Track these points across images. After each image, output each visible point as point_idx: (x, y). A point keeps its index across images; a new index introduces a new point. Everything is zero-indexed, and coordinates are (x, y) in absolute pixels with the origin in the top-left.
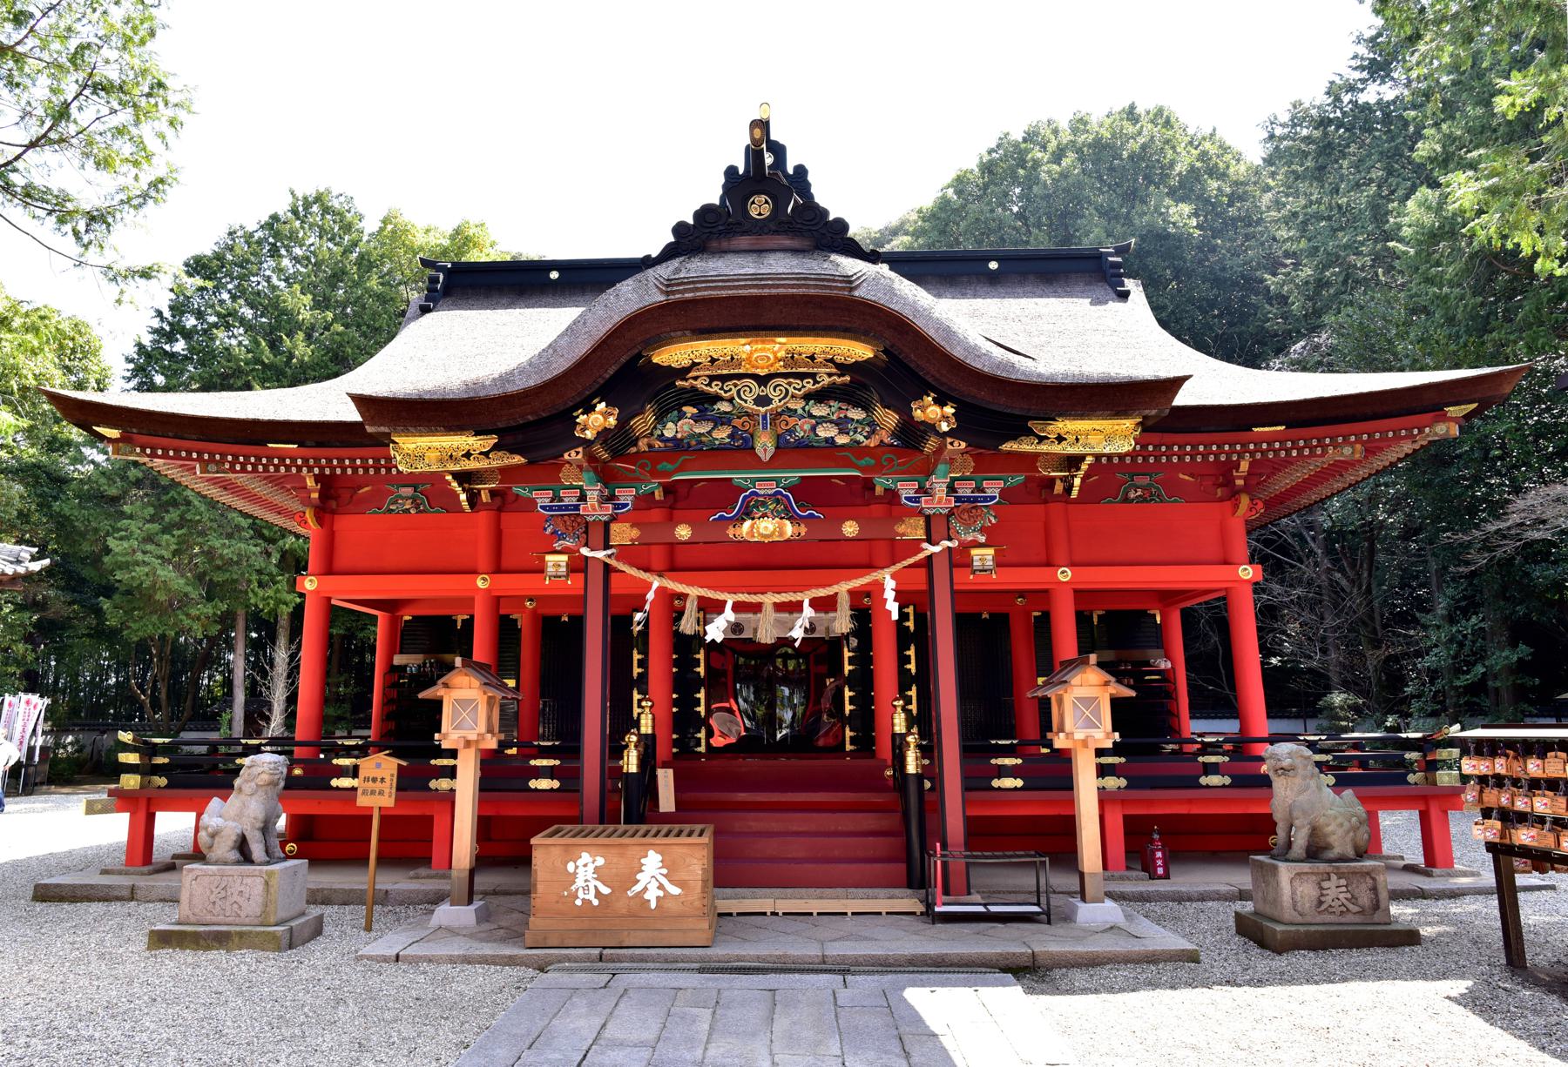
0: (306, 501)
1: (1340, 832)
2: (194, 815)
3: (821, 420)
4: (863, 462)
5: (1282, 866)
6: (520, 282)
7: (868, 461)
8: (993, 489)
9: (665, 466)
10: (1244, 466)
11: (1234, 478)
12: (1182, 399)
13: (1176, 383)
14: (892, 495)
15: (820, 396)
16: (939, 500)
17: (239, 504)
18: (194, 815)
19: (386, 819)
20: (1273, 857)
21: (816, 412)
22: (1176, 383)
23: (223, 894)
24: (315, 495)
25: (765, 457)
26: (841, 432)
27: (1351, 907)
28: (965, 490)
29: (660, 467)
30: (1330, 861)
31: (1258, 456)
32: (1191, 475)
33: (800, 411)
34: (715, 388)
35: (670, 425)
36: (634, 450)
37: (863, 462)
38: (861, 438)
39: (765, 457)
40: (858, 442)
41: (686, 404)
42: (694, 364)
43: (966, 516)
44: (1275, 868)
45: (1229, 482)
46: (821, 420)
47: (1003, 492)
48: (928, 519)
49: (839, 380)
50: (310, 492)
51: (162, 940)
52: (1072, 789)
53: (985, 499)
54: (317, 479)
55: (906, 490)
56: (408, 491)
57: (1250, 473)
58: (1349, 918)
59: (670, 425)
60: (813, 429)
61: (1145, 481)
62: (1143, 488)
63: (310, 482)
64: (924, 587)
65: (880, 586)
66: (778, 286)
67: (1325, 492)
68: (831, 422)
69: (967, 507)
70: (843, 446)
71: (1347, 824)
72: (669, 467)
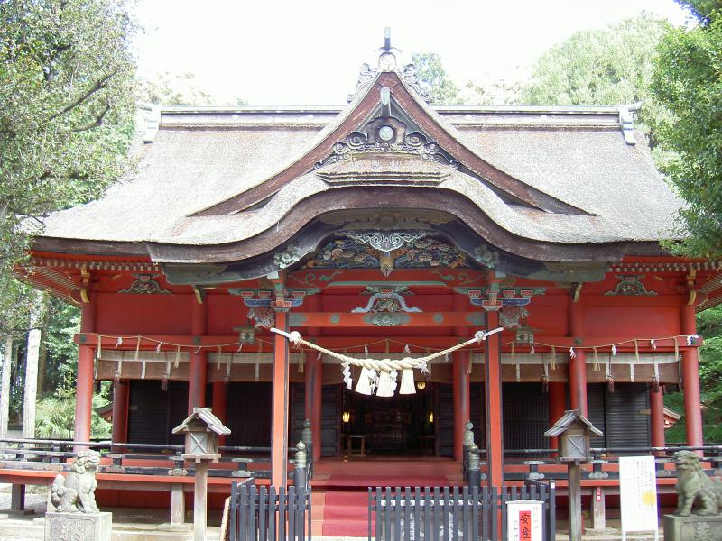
2: (401, 392)
4: (447, 278)
6: (258, 121)
7: (449, 277)
8: (527, 297)
9: (324, 278)
10: (693, 273)
16: (492, 305)
17: (55, 442)
18: (401, 392)
24: (86, 281)
25: (387, 274)
26: (434, 259)
28: (510, 296)
29: (320, 279)
36: (305, 267)
37: (447, 278)
38: (445, 262)
39: (387, 274)
40: (445, 265)
43: (509, 312)
46: (422, 251)
47: (532, 299)
48: (486, 314)
52: (620, 519)
54: (88, 270)
55: (474, 297)
56: (146, 279)
60: (417, 256)
61: (629, 280)
63: (84, 273)
65: (510, 345)
68: (428, 252)
69: (509, 308)
70: (434, 267)
72: (326, 278)
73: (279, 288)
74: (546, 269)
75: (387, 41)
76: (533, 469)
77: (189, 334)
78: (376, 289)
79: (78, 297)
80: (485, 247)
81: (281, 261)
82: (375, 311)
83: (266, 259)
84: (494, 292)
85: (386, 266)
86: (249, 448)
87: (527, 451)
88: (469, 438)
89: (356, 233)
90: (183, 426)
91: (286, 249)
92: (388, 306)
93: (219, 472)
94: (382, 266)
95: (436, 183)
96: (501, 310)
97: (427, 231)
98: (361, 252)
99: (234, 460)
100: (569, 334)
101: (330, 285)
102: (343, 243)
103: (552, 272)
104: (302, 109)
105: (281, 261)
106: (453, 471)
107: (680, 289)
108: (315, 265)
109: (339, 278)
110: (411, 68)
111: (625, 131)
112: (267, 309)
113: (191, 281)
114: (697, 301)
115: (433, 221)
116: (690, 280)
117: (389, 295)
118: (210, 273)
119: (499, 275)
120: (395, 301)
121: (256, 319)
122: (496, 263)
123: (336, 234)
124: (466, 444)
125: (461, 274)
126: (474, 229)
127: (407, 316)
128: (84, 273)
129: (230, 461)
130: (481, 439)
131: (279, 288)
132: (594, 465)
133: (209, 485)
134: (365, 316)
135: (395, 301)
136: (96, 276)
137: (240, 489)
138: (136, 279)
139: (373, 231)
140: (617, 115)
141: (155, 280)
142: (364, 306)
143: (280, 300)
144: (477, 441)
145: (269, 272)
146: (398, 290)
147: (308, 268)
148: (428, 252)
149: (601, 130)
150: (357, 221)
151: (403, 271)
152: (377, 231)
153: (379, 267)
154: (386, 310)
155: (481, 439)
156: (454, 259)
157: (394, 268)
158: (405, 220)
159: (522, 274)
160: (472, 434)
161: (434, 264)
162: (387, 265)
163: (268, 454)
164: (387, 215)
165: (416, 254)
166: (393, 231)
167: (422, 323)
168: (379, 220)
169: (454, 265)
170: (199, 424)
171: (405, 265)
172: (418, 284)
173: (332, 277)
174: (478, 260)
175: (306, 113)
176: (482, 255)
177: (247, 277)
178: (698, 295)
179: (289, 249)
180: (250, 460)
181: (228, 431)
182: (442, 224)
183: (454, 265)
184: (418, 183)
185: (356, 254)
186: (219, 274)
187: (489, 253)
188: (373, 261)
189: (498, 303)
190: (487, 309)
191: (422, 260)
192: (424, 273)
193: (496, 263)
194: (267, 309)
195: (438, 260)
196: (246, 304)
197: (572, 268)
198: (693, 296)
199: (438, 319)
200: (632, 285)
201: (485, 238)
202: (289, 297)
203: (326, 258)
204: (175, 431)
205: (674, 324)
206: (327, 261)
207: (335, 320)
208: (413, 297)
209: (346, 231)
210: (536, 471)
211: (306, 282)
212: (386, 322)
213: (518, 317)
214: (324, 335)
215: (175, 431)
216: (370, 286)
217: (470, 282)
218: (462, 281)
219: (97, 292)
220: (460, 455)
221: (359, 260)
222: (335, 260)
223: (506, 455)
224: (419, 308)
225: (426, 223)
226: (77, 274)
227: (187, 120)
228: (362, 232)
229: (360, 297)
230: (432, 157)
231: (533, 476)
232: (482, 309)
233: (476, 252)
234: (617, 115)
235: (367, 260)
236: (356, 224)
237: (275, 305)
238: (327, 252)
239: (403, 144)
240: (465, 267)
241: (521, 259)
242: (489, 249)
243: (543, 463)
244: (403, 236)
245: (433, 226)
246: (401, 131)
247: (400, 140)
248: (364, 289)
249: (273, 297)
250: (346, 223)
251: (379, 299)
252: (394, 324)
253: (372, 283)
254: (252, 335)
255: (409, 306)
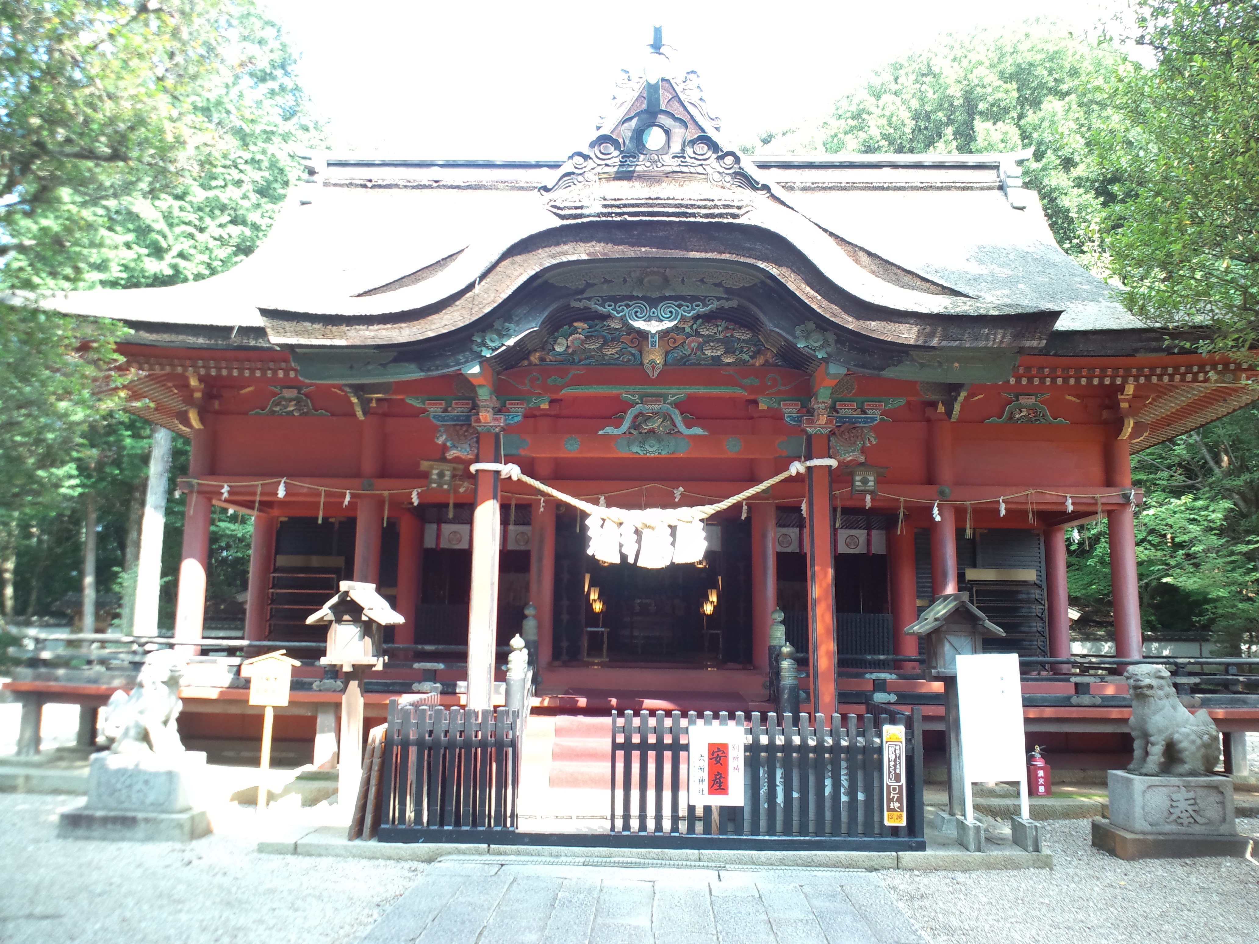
0: (189, 400)
1: (1193, 748)
3: (708, 339)
5: (1136, 778)
8: (875, 412)
10: (1130, 389)
11: (1118, 403)
12: (1062, 325)
13: (1056, 315)
14: (776, 416)
15: (707, 318)
16: (821, 424)
19: (280, 719)
20: (1129, 772)
21: (704, 332)
22: (1056, 315)
23: (128, 782)
24: (198, 395)
26: (727, 352)
27: (1198, 819)
28: (848, 411)
29: (549, 381)
30: (1181, 775)
31: (1142, 380)
32: (1076, 396)
33: (688, 330)
34: (607, 309)
35: (561, 340)
36: (526, 363)
37: (747, 382)
38: (746, 357)
40: (745, 362)
41: (576, 321)
42: (589, 285)
44: (1129, 781)
45: (1114, 406)
46: (708, 339)
48: (809, 437)
49: (726, 304)
50: (192, 391)
51: (75, 823)
53: (866, 420)
54: (201, 379)
55: (790, 411)
57: (1134, 396)
58: (1197, 829)
59: (561, 340)
60: (700, 347)
61: (1028, 401)
62: (1029, 409)
63: (194, 382)
64: (524, 826)
66: (693, 215)
67: (1212, 416)
68: (718, 340)
69: (845, 429)
70: (729, 364)
71: (1199, 742)
72: (560, 382)
73: (484, 394)
74: (913, 360)
75: (658, 32)
76: (880, 686)
77: (357, 475)
78: (636, 398)
79: (184, 420)
80: (811, 325)
81: (484, 344)
82: (635, 432)
83: (460, 340)
84: (823, 397)
85: (652, 362)
86: (440, 647)
87: (869, 657)
88: (778, 634)
89: (605, 300)
90: (325, 612)
91: (492, 326)
92: (655, 424)
93: (393, 684)
94: (646, 361)
95: (735, 216)
96: (832, 433)
97: (719, 299)
98: (613, 340)
99: (416, 665)
100: (930, 479)
101: (564, 391)
102: (586, 326)
103: (922, 366)
104: (533, 159)
105: (484, 344)
106: (749, 682)
107: (1105, 414)
108: (542, 359)
109: (578, 381)
110: (692, 76)
111: (1008, 190)
112: (465, 427)
113: (339, 380)
114: (1136, 433)
115: (729, 284)
116: (1125, 401)
117: (656, 407)
118: (368, 363)
119: (836, 370)
120: (667, 417)
121: (449, 444)
122: (829, 349)
123: (575, 304)
124: (775, 643)
125: (769, 376)
126: (797, 293)
127: (685, 440)
128: (194, 382)
129: (411, 667)
130: (799, 634)
131: (484, 394)
132: (1077, 685)
133: (366, 705)
134: (619, 440)
135: (667, 417)
136: (214, 389)
137: (405, 713)
138: (275, 394)
139: (632, 298)
140: (997, 167)
141: (305, 395)
142: (617, 426)
143: (486, 416)
144: (789, 638)
145: (466, 362)
146: (671, 399)
147: (530, 364)
148: (718, 340)
149: (972, 188)
150: (606, 281)
151: (678, 370)
152: (637, 298)
153: (642, 364)
154: (652, 431)
155: (799, 634)
156: (758, 353)
157: (665, 364)
158: (683, 281)
159: (874, 368)
160: (782, 628)
161: (729, 360)
162: (655, 357)
163: (463, 657)
164: (654, 273)
165: (699, 343)
166: (664, 298)
167: (705, 453)
168: (641, 281)
169: (759, 361)
170: (350, 610)
171: (684, 361)
172: (701, 390)
173: (567, 379)
174: (801, 345)
175: (538, 166)
176: (807, 338)
177: (429, 370)
178: (1136, 423)
179: (497, 325)
180: (441, 666)
181: (398, 619)
182: (744, 288)
183: (759, 361)
184: (706, 216)
185: (605, 343)
186: (384, 366)
187: (816, 336)
188: (633, 355)
189: (829, 422)
190: (810, 430)
191: (709, 353)
192: (712, 372)
193: (829, 349)
194: (465, 427)
195: (734, 353)
196: (435, 421)
197: (958, 360)
198: (1129, 425)
199: (733, 447)
200: (1029, 409)
201: (815, 307)
202: (499, 411)
203: (559, 349)
204: (311, 620)
205: (1096, 470)
206: (560, 354)
207: (572, 448)
208: (692, 410)
209: (589, 299)
210: (884, 691)
211: (528, 387)
212: (652, 450)
213: (859, 444)
214: (560, 475)
215: (311, 620)
216: (626, 393)
217: (783, 388)
218: (770, 387)
219: (217, 413)
220: (763, 659)
221: (610, 351)
222: (574, 352)
223: (841, 663)
224: (703, 428)
225: (716, 285)
226: (184, 386)
227: (366, 173)
228: (615, 300)
229: (614, 411)
230: (728, 178)
231: (880, 697)
232: (804, 431)
233: (798, 333)
234: (997, 167)
235: (621, 353)
236: (605, 287)
237: (478, 420)
238: (560, 340)
239: (681, 155)
240: (776, 365)
241: (866, 352)
242: (818, 326)
243: (894, 676)
244: (679, 306)
245: (728, 291)
246: (678, 133)
247: (676, 147)
248: (617, 398)
249: (475, 407)
250: (589, 285)
251: (641, 414)
252: (664, 453)
253: (631, 388)
254: (448, 473)
255: (689, 426)
